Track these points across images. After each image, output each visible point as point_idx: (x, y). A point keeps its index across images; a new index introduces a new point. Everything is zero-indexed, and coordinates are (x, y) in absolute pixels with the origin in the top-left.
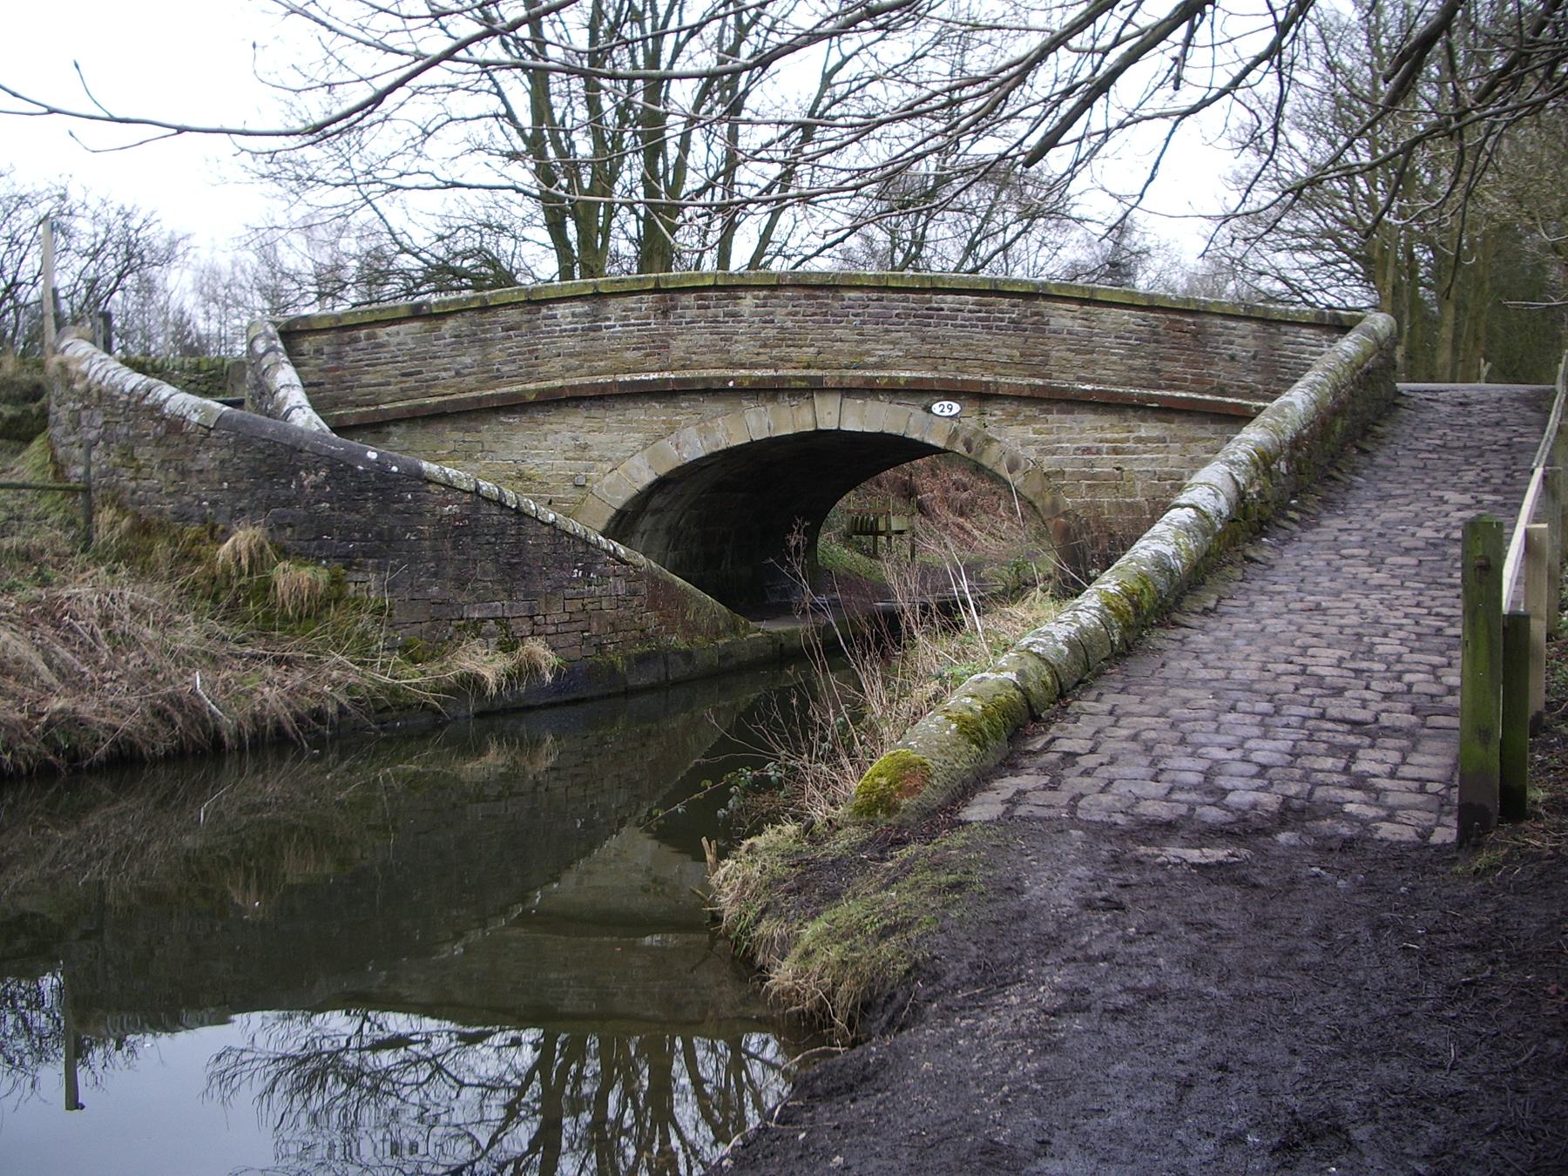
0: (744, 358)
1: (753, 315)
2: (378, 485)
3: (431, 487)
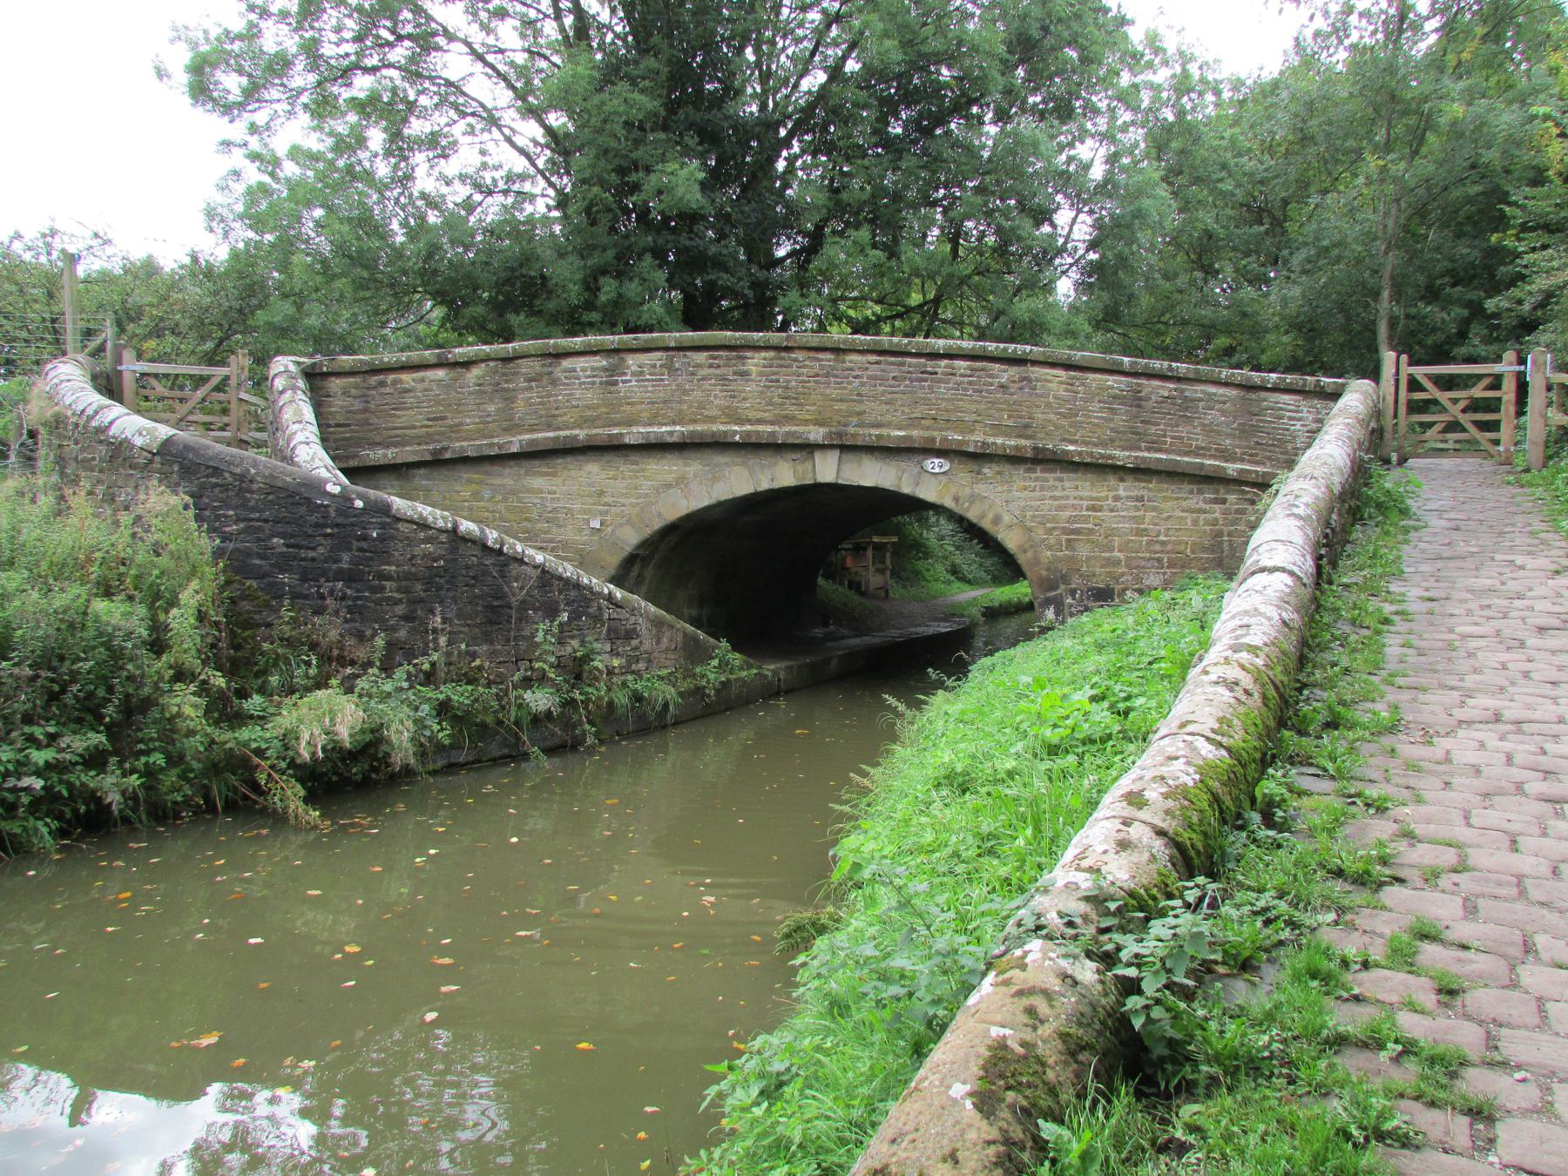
0: (751, 415)
1: (761, 374)
2: (340, 520)
3: (400, 526)
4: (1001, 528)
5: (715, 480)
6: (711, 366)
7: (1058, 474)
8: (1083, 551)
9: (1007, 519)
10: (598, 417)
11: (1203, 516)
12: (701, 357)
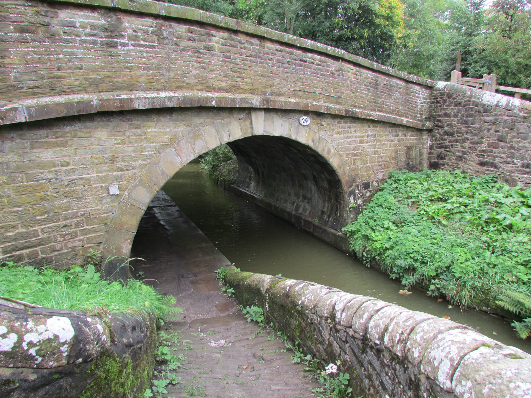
0: (216, 84)
4: (331, 156)
5: (196, 137)
6: (190, 39)
7: (349, 124)
8: (359, 164)
9: (333, 150)
10: (102, 81)
11: (393, 143)
12: (182, 29)
